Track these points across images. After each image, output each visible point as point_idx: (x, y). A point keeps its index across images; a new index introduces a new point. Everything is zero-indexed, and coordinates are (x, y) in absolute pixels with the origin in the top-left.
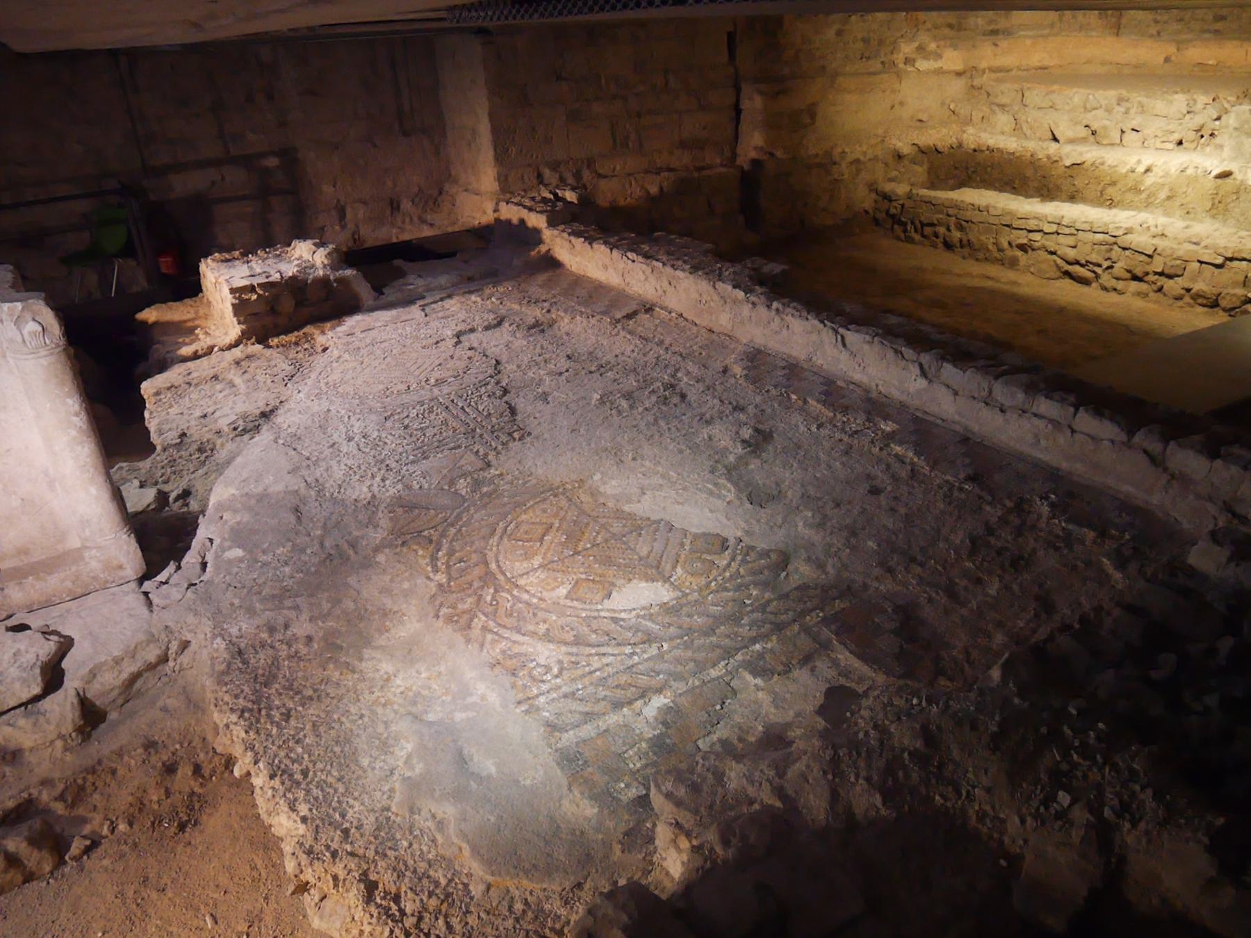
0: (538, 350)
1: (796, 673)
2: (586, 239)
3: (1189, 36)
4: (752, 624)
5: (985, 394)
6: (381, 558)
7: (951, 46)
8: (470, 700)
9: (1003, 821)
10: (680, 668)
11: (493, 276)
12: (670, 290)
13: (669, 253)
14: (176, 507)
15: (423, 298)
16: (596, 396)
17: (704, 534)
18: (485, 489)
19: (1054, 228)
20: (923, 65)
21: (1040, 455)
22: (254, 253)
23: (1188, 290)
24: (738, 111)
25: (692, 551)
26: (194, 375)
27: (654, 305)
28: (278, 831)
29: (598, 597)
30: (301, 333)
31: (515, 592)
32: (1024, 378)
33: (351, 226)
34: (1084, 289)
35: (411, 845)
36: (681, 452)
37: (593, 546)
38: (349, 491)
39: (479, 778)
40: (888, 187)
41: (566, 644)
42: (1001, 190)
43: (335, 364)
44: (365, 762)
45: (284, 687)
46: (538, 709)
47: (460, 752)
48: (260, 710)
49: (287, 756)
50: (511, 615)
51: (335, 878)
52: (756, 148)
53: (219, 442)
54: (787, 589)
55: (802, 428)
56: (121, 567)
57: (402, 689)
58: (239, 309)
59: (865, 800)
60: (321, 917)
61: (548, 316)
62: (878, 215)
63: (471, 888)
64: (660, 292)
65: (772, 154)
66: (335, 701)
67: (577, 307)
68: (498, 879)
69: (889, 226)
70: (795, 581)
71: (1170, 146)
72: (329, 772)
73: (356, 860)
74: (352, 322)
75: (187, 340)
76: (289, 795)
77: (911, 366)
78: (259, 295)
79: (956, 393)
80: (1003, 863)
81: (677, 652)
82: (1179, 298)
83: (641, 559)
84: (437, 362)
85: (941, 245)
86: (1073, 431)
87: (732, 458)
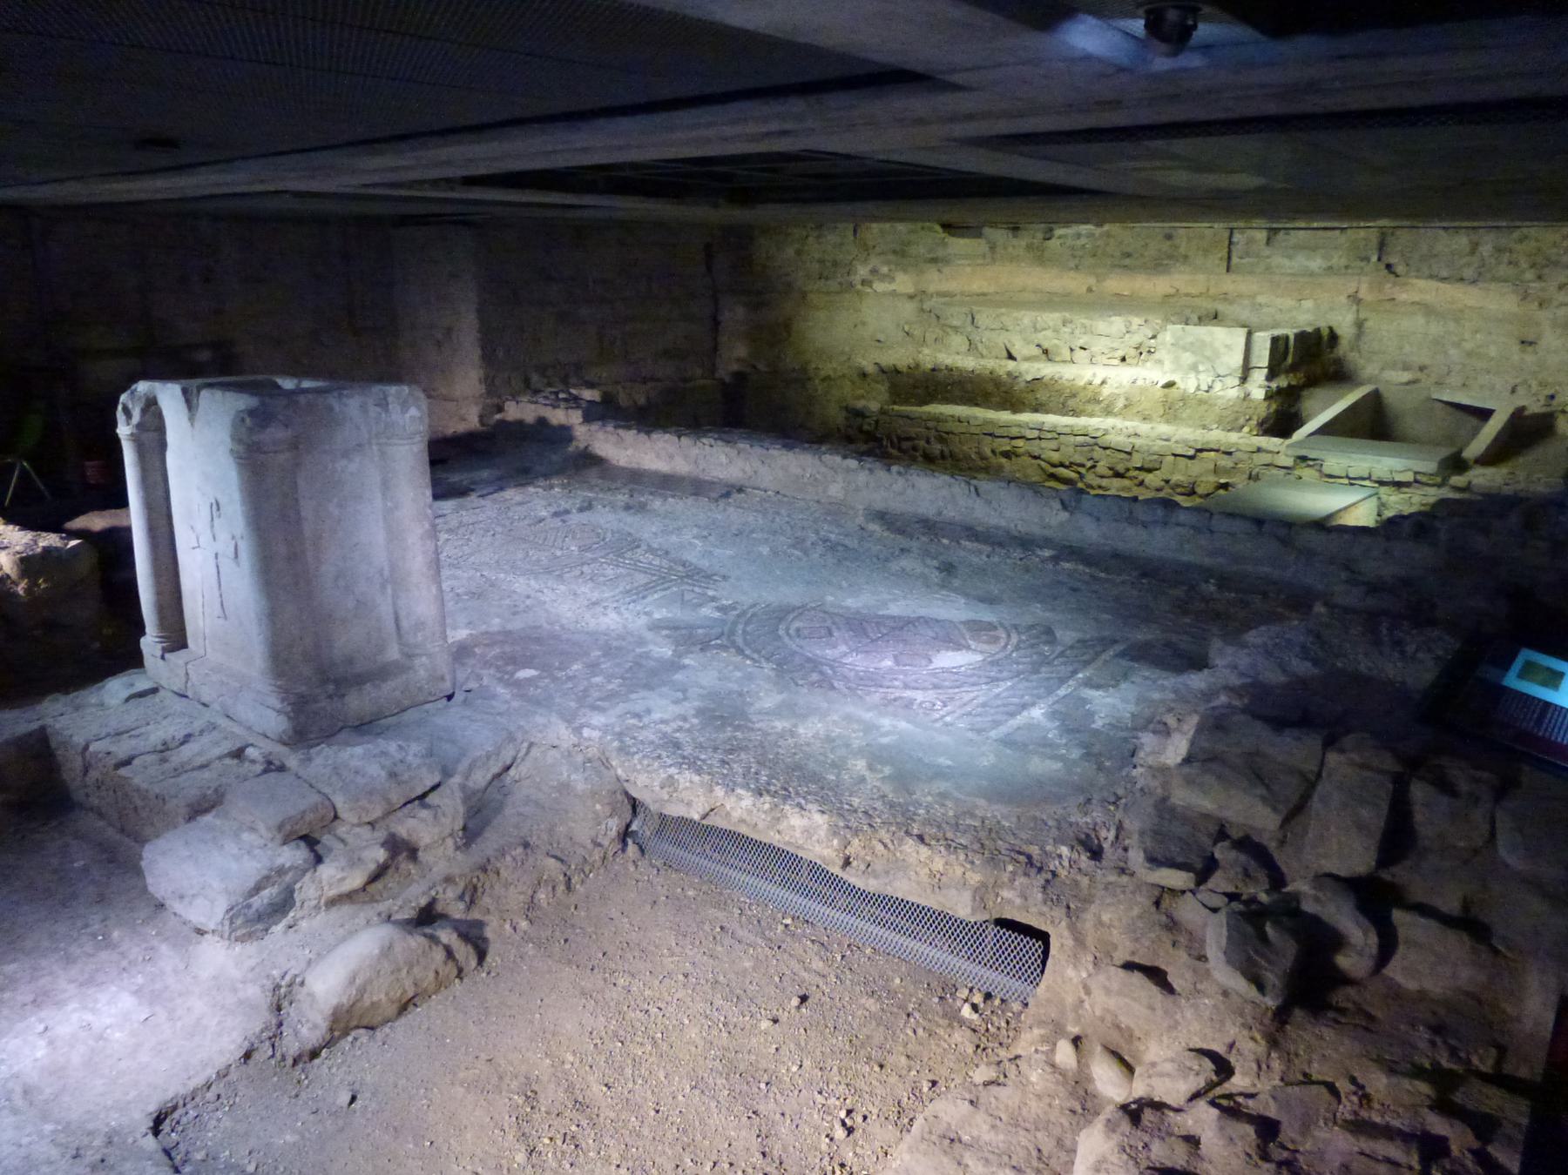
19: (1035, 434)
20: (880, 287)
23: (1167, 482)
24: (716, 323)
40: (860, 404)
52: (738, 360)
62: (851, 432)
65: (754, 367)
71: (1116, 362)
79: (1098, 519)
86: (1212, 532)
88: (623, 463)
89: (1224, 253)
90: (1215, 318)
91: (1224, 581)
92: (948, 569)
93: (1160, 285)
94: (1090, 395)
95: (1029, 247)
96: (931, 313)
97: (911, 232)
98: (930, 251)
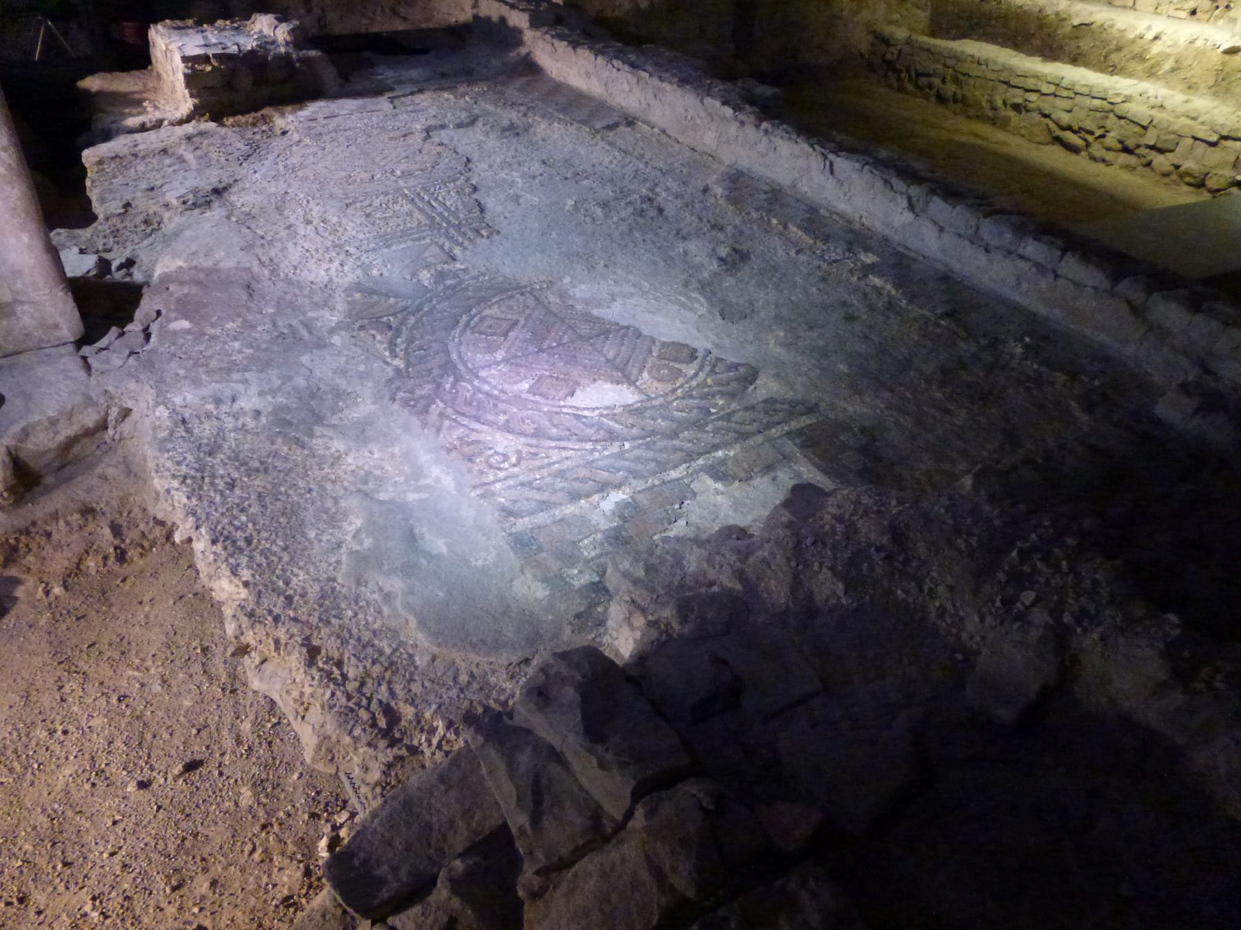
0: (512, 152)
1: (757, 481)
2: (570, 43)
4: (716, 431)
6: (336, 340)
8: (423, 482)
9: (962, 619)
10: (640, 467)
11: (468, 75)
12: (654, 103)
13: (656, 64)
14: (118, 276)
15: (392, 89)
16: (571, 202)
17: (673, 343)
18: (449, 282)
19: (1052, 89)
21: (1018, 299)
22: (211, 22)
23: (1177, 167)
25: (659, 357)
26: (141, 147)
27: (635, 118)
28: (218, 596)
29: (561, 394)
30: (259, 114)
31: (476, 383)
32: (1015, 219)
33: (317, 11)
34: (1074, 158)
35: (356, 615)
36: (655, 263)
37: (559, 345)
38: (305, 272)
39: (429, 556)
40: (888, 30)
41: (525, 435)
42: (1003, 45)
43: (294, 148)
44: (312, 534)
45: (229, 458)
46: (493, 494)
47: (411, 530)
48: (203, 478)
49: (231, 523)
50: (470, 405)
51: (277, 642)
53: (166, 215)
54: (753, 401)
55: (780, 253)
56: (56, 326)
57: (353, 467)
58: (191, 80)
59: (827, 587)
60: (261, 679)
61: (524, 120)
63: (417, 658)
64: (644, 106)
66: (282, 475)
67: (556, 114)
68: (445, 651)
70: (762, 394)
71: (1184, 14)
72: (274, 542)
73: (299, 625)
74: (314, 108)
75: (134, 111)
76: (232, 561)
77: (899, 197)
78: (214, 67)
79: (941, 229)
80: (959, 657)
81: (638, 452)
82: (1166, 175)
83: (608, 361)
84: (404, 155)
85: (933, 99)
86: (1057, 276)
87: (706, 274)
88: (554, 75)
94: (1137, 50)
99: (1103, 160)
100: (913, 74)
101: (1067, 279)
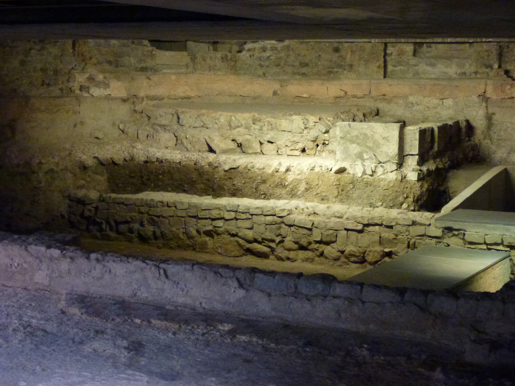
3: (285, 77)
5: (292, 290)
7: (115, 77)
19: (233, 215)
20: (96, 92)
21: (343, 326)
23: (342, 252)
34: (266, 261)
40: (81, 193)
69: (84, 227)
71: (297, 153)
77: (230, 282)
79: (269, 295)
82: (337, 259)
85: (136, 240)
86: (363, 302)
89: (381, 62)
90: (377, 114)
91: (375, 345)
92: (136, 348)
93: (332, 89)
94: (277, 180)
95: (224, 59)
96: (142, 113)
97: (124, 45)
98: (141, 61)
99: (288, 259)
100: (113, 224)
101: (371, 302)
